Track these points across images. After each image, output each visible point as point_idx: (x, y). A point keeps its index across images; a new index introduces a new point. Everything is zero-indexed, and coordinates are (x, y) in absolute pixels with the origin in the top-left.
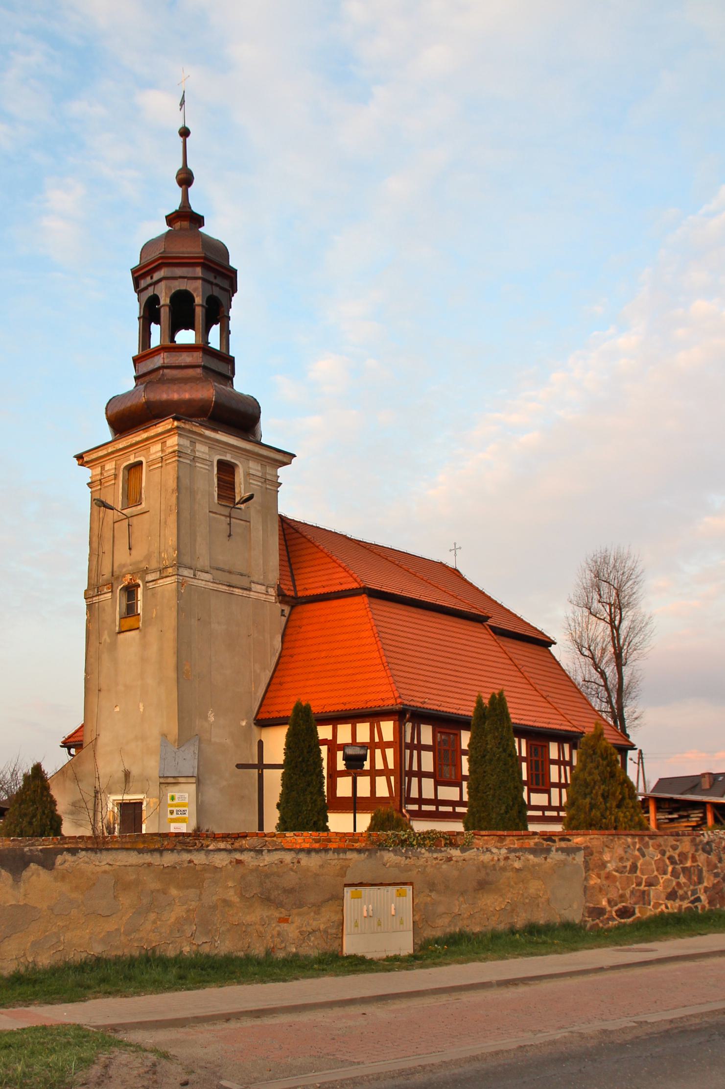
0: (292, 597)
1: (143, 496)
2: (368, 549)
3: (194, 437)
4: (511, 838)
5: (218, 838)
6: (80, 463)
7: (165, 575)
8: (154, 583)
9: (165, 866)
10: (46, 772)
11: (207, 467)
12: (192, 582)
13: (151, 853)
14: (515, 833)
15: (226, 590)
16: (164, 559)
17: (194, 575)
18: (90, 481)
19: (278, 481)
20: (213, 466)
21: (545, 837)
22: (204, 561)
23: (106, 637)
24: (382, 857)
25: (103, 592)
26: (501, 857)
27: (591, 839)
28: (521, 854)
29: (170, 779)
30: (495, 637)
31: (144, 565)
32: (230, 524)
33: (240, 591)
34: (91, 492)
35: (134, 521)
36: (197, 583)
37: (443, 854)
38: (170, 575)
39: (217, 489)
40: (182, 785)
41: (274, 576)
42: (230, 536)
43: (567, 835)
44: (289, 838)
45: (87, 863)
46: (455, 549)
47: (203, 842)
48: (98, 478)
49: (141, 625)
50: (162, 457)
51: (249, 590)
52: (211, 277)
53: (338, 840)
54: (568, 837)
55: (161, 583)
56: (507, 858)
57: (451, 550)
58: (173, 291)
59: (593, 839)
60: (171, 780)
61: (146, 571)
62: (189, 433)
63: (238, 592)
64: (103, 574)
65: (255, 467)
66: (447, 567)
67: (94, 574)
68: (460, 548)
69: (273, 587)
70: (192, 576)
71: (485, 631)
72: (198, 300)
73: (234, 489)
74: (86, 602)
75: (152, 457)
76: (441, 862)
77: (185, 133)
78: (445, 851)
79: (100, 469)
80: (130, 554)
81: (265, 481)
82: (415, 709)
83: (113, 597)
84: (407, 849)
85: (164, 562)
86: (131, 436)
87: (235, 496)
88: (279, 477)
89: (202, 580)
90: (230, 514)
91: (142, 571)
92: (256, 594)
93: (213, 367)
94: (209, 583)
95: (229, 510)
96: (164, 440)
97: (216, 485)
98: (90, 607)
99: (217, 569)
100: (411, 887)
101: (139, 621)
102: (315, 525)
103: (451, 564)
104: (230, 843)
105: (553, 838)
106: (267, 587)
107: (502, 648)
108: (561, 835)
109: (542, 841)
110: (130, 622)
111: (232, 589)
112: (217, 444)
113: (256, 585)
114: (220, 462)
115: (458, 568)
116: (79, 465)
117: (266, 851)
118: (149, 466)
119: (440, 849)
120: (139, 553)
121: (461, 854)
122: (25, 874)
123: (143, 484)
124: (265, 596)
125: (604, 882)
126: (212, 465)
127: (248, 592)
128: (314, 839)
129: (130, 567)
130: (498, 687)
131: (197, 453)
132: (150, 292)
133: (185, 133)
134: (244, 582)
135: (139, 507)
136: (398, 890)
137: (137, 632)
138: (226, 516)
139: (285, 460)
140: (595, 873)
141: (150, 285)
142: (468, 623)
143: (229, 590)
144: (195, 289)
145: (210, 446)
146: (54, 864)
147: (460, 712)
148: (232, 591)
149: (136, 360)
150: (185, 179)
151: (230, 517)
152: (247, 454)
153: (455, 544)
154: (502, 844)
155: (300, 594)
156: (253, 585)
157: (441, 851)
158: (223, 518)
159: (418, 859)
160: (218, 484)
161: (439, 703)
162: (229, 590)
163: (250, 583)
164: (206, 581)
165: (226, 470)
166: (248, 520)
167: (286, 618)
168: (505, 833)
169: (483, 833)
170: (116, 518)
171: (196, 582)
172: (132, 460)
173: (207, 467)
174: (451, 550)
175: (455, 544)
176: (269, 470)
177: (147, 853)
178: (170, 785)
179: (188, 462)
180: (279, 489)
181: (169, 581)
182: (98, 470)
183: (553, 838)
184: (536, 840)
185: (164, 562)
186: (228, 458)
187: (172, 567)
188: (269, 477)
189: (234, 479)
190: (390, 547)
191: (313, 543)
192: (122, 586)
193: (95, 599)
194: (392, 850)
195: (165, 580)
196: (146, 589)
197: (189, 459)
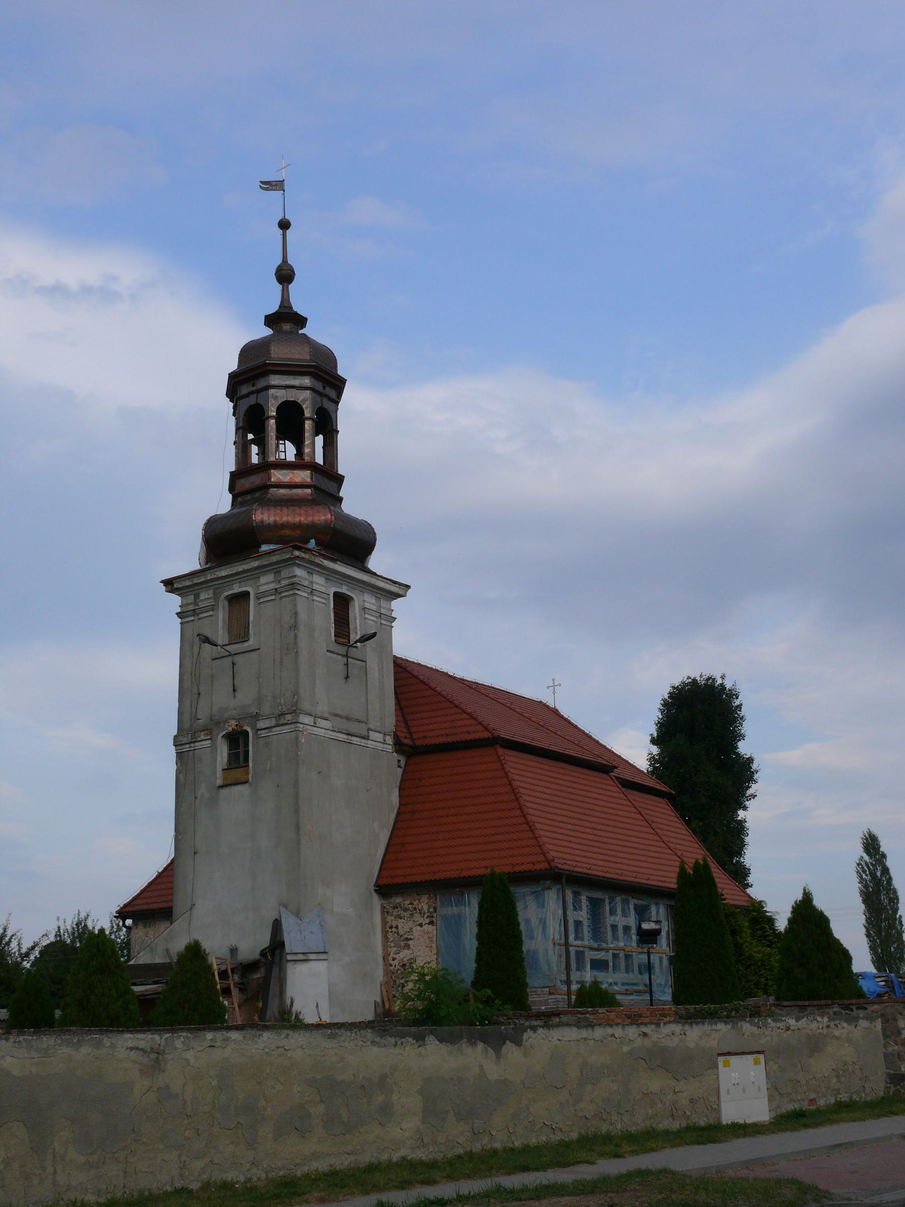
0: (410, 746)
1: (251, 631)
2: (474, 689)
3: (312, 567)
4: (812, 1008)
5: (532, 1016)
6: (167, 590)
7: (282, 722)
8: (268, 730)
9: (596, 1040)
10: (207, 952)
11: (324, 601)
12: (313, 731)
13: (586, 1029)
14: (815, 1003)
15: (345, 739)
16: (280, 704)
17: (314, 723)
18: (179, 610)
19: (392, 615)
20: (330, 600)
21: (843, 1006)
22: (323, 708)
23: (203, 791)
24: (741, 1026)
25: (199, 739)
26: (825, 1025)
27: (885, 1007)
28: (838, 1022)
29: (299, 955)
30: (623, 789)
31: (254, 710)
32: (347, 664)
33: (358, 739)
34: (181, 623)
35: (239, 659)
36: (317, 732)
37: (784, 1023)
38: (289, 722)
39: (333, 625)
40: (312, 962)
41: (390, 722)
42: (347, 677)
43: (863, 1004)
44: (601, 1014)
45: (543, 1039)
46: (554, 686)
47: (517, 1021)
48: (191, 607)
49: (250, 778)
50: (276, 589)
51: (367, 738)
52: (319, 386)
53: (648, 1015)
54: (864, 1005)
55: (275, 731)
56: (828, 1027)
57: (548, 687)
58: (280, 402)
59: (888, 1006)
60: (301, 957)
61: (256, 717)
62: (307, 563)
63: (357, 741)
64: (198, 718)
65: (370, 601)
66: (548, 707)
67: (186, 718)
68: (560, 685)
69: (390, 735)
70: (313, 724)
71: (612, 783)
72: (307, 414)
73: (348, 625)
74: (176, 750)
75: (262, 589)
76: (782, 1031)
77: (284, 225)
78: (785, 1020)
79: (192, 597)
80: (235, 697)
81: (380, 616)
82: (569, 873)
83: (214, 748)
84: (759, 1019)
85: (280, 708)
86: (237, 564)
87: (349, 632)
88: (393, 610)
89: (322, 728)
90: (347, 652)
91: (251, 716)
92: (374, 743)
93: (323, 487)
94: (329, 731)
95: (346, 648)
96: (278, 570)
97: (333, 621)
98: (180, 755)
99: (335, 715)
100: (763, 1056)
101: (247, 773)
102: (434, 667)
103: (551, 704)
104: (543, 1021)
105: (851, 1007)
106: (315, 717)
107: (631, 802)
108: (858, 1004)
109: (840, 1010)
110: (237, 774)
111: (350, 737)
112: (334, 575)
113: (374, 733)
114: (336, 595)
115: (557, 707)
116: (167, 591)
117: (662, 1024)
118: (259, 599)
119: (781, 1019)
120: (246, 697)
121: (796, 1024)
122: (504, 1049)
123: (251, 618)
124: (382, 745)
125: (901, 1049)
126: (329, 599)
127: (365, 741)
128: (625, 1015)
129: (235, 712)
130: (693, 855)
131: (314, 585)
132: (252, 400)
133: (284, 225)
134: (361, 729)
135: (246, 645)
136: (754, 1059)
137: (246, 786)
138: (342, 655)
139: (401, 592)
140: (892, 1040)
141: (252, 393)
142: (541, 760)
143: (348, 739)
144: (304, 400)
145: (327, 577)
146: (522, 1041)
147: (608, 875)
148: (351, 740)
149: (234, 476)
150: (285, 276)
151: (347, 656)
152: (362, 586)
153: (554, 680)
154: (802, 1014)
155: (418, 743)
156: (371, 733)
157: (782, 1021)
158: (340, 657)
159: (766, 1028)
160: (335, 620)
161: (588, 866)
162: (348, 739)
163: (368, 730)
164: (326, 729)
165: (342, 603)
166: (364, 660)
167: (402, 770)
168: (807, 1003)
169: (785, 1003)
170: (215, 655)
171: (315, 730)
172: (237, 589)
173: (324, 601)
174: (548, 687)
175: (554, 680)
176: (383, 603)
177: (583, 1028)
178: (298, 962)
179: (305, 595)
180: (393, 624)
181: (288, 729)
182: (191, 598)
183: (851, 1007)
184: (835, 1009)
185: (280, 708)
186: (344, 590)
187: (291, 713)
188: (383, 611)
189: (348, 613)
190: (490, 685)
191: (427, 685)
192: (224, 733)
193: (186, 748)
194: (748, 1021)
195: (282, 728)
196: (257, 736)
197: (375, 616)
